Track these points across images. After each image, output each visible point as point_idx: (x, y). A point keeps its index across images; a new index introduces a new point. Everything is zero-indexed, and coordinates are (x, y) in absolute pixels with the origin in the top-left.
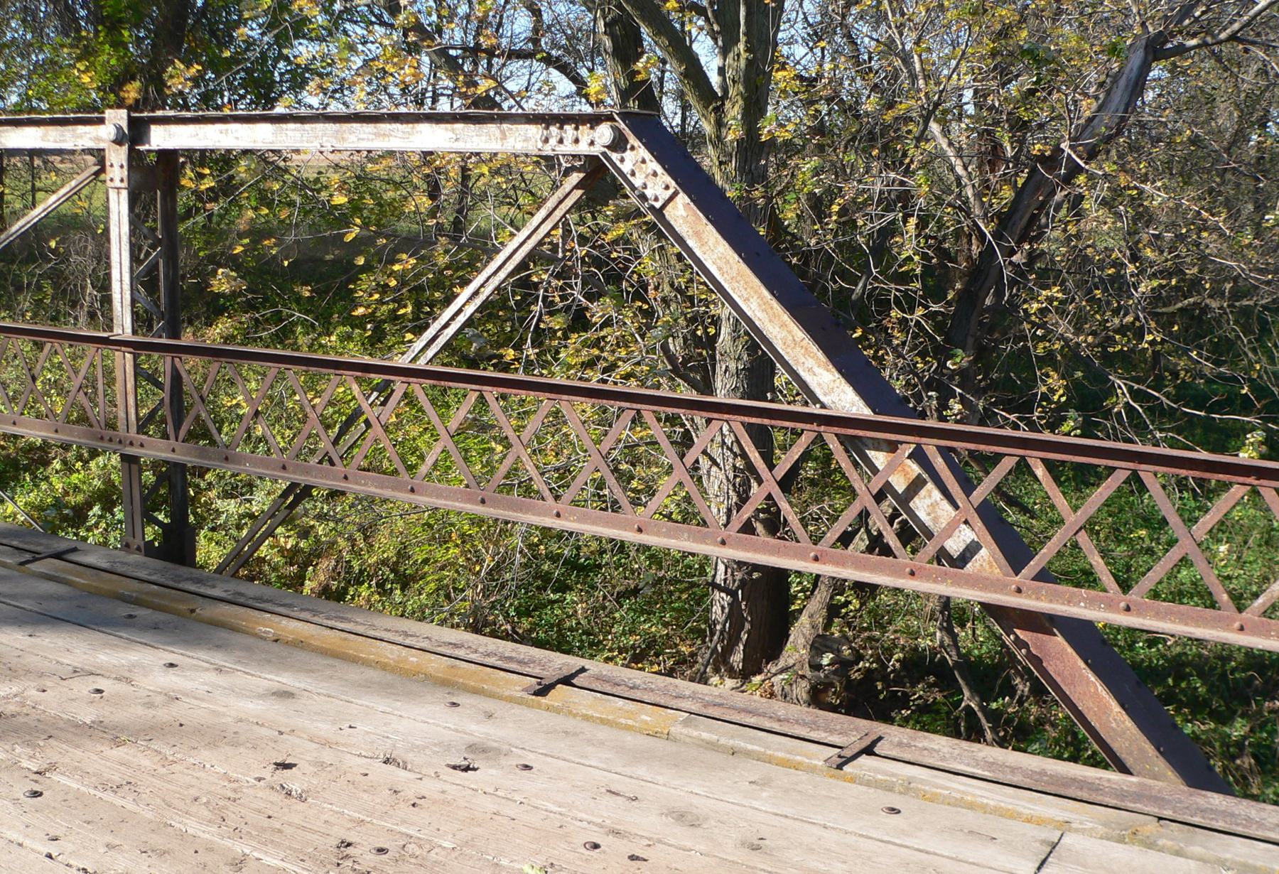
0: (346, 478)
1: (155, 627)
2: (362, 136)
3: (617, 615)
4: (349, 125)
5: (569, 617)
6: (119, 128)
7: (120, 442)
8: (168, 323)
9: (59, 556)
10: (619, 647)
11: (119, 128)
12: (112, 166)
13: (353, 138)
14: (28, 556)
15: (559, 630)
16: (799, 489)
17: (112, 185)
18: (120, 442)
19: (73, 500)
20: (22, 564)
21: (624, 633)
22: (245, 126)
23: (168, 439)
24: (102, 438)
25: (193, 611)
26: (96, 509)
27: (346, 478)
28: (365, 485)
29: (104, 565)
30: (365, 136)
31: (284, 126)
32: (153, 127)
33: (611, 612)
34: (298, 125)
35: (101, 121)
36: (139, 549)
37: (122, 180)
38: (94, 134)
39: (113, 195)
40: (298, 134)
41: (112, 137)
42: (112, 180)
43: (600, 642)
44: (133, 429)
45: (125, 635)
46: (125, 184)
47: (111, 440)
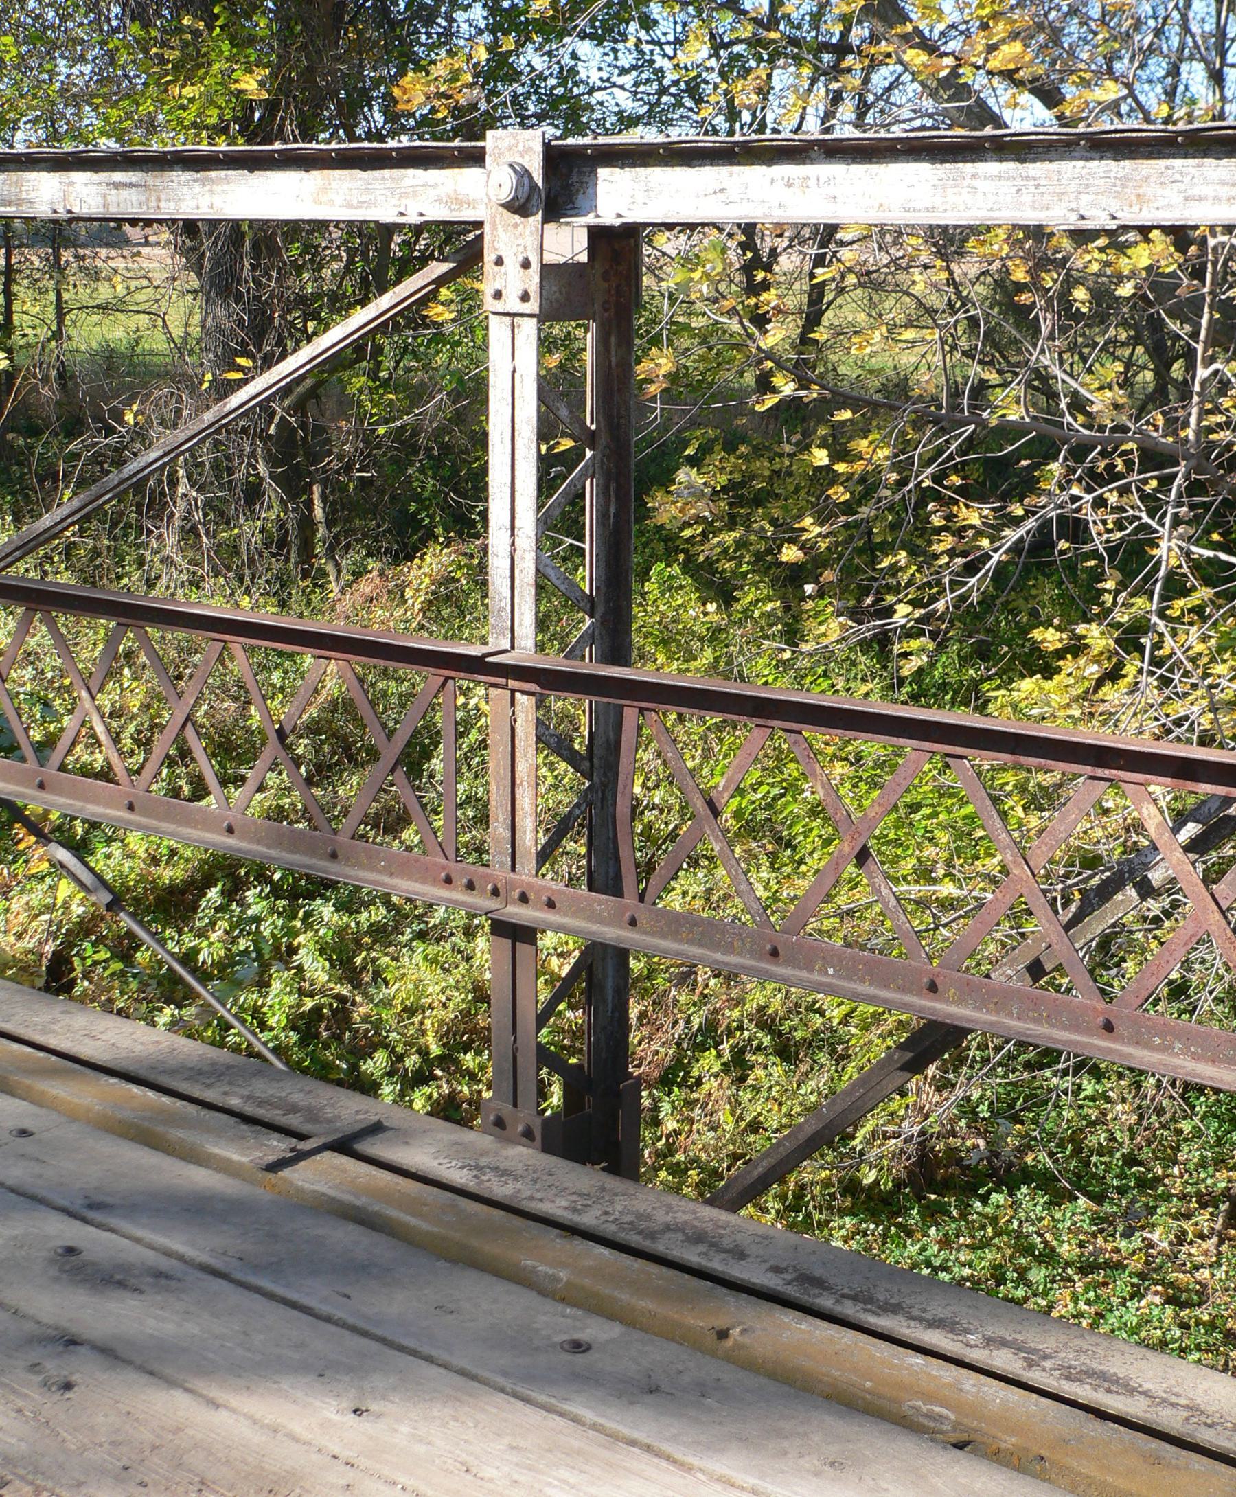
0: (1108, 1027)
1: (648, 1390)
2: (1195, 191)
3: (1186, 1126)
4: (1161, 164)
5: (1092, 1124)
6: (523, 174)
7: (495, 892)
8: (603, 622)
9: (344, 1146)
10: (1199, 1194)
11: (523, 174)
12: (499, 262)
13: (1171, 195)
14: (278, 1146)
15: (1077, 1151)
16: (642, 657)
17: (499, 306)
18: (495, 892)
19: (167, 875)
20: (274, 1167)
21: (1202, 1164)
22: (858, 170)
23: (617, 891)
24: (448, 880)
25: (723, 1334)
26: (213, 894)
27: (1108, 1027)
28: (1163, 1049)
29: (460, 1177)
30: (1208, 191)
31: (968, 168)
32: (603, 172)
33: (1174, 1119)
34: (1010, 167)
35: (476, 158)
36: (528, 1134)
37: (525, 297)
38: (443, 191)
39: (498, 331)
40: (1007, 188)
41: (505, 194)
42: (498, 295)
43: (1158, 1180)
44: (527, 864)
45: (589, 1416)
46: (533, 306)
47: (470, 886)
